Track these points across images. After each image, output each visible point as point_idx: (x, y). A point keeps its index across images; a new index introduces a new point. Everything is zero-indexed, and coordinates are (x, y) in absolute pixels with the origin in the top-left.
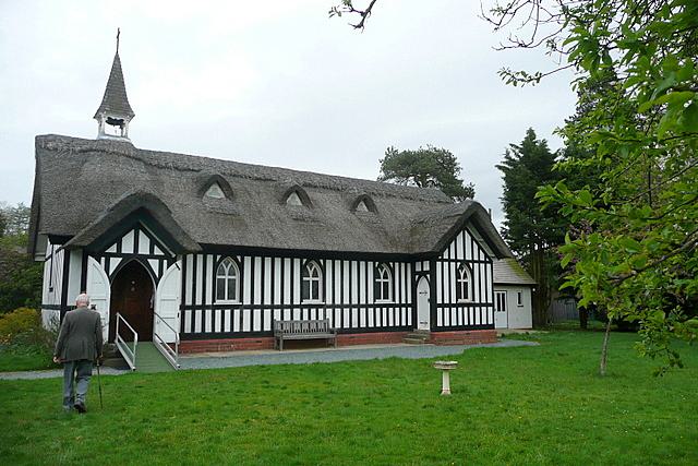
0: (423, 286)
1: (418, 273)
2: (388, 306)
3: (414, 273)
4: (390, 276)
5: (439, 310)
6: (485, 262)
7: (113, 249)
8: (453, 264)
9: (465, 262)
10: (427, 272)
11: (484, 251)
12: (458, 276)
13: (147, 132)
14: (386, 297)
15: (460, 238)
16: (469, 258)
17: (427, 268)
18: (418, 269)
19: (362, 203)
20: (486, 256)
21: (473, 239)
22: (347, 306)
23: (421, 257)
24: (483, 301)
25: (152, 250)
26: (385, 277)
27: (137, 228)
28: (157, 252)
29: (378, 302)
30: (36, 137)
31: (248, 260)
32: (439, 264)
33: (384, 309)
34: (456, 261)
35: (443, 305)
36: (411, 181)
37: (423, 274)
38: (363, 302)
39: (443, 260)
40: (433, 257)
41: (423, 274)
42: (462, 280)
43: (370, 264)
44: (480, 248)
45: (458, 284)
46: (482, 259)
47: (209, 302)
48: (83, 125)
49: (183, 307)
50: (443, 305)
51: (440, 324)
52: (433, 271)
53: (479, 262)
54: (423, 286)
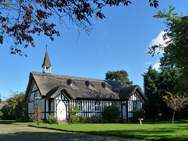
0: (124, 107)
1: (123, 104)
3: (122, 104)
5: (129, 113)
6: (140, 101)
7: (57, 99)
10: (125, 104)
14: (98, 110)
17: (125, 102)
18: (123, 103)
20: (140, 99)
26: (135, 105)
28: (66, 99)
30: (31, 73)
31: (101, 101)
33: (98, 113)
41: (124, 104)
43: (94, 101)
44: (139, 97)
46: (139, 100)
53: (139, 101)
54: (124, 107)
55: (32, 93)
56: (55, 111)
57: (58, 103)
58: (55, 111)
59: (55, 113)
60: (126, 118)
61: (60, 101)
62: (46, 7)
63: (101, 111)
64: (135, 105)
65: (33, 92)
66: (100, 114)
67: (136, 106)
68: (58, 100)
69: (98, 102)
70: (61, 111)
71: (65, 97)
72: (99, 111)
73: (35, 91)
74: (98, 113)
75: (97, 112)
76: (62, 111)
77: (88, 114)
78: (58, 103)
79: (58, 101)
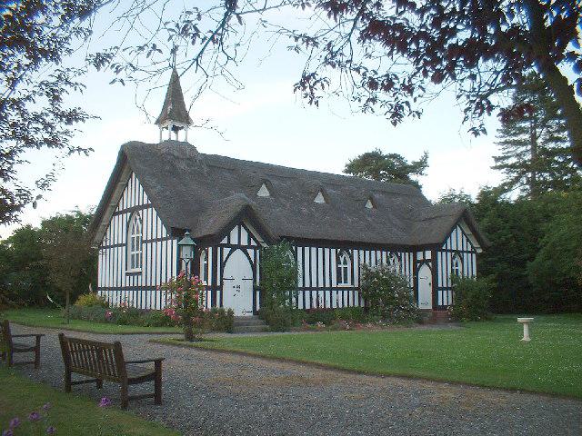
0: (425, 272)
1: (419, 262)
2: (348, 289)
4: (460, 264)
5: (440, 292)
7: (225, 241)
8: (449, 254)
9: (457, 252)
11: (255, 239)
12: (338, 262)
13: (204, 140)
15: (453, 234)
16: (460, 249)
17: (428, 255)
19: (264, 186)
21: (463, 233)
22: (307, 289)
23: (423, 248)
24: (314, 285)
25: (249, 242)
27: (241, 224)
28: (253, 243)
29: (340, 285)
32: (439, 253)
33: (346, 292)
34: (451, 251)
35: (443, 289)
36: (352, 175)
37: (425, 261)
38: (321, 285)
39: (442, 251)
40: (436, 247)
41: (425, 261)
42: (342, 266)
43: (384, 253)
45: (339, 270)
47: (334, 285)
48: (152, 135)
49: (221, 288)
50: (443, 289)
51: (440, 304)
52: (434, 259)
53: (468, 252)
54: (425, 272)
55: (115, 214)
56: (219, 284)
57: (227, 258)
58: (219, 284)
59: (218, 292)
60: (430, 307)
61: (234, 248)
62: (176, 129)
63: (356, 285)
64: (345, 263)
65: (122, 212)
66: (296, 282)
67: (349, 266)
68: (228, 245)
69: (395, 257)
70: (235, 283)
71: (250, 236)
72: (349, 285)
73: (134, 210)
74: (346, 292)
75: (343, 289)
76: (241, 283)
77: (314, 293)
78: (227, 258)
79: (227, 251)
